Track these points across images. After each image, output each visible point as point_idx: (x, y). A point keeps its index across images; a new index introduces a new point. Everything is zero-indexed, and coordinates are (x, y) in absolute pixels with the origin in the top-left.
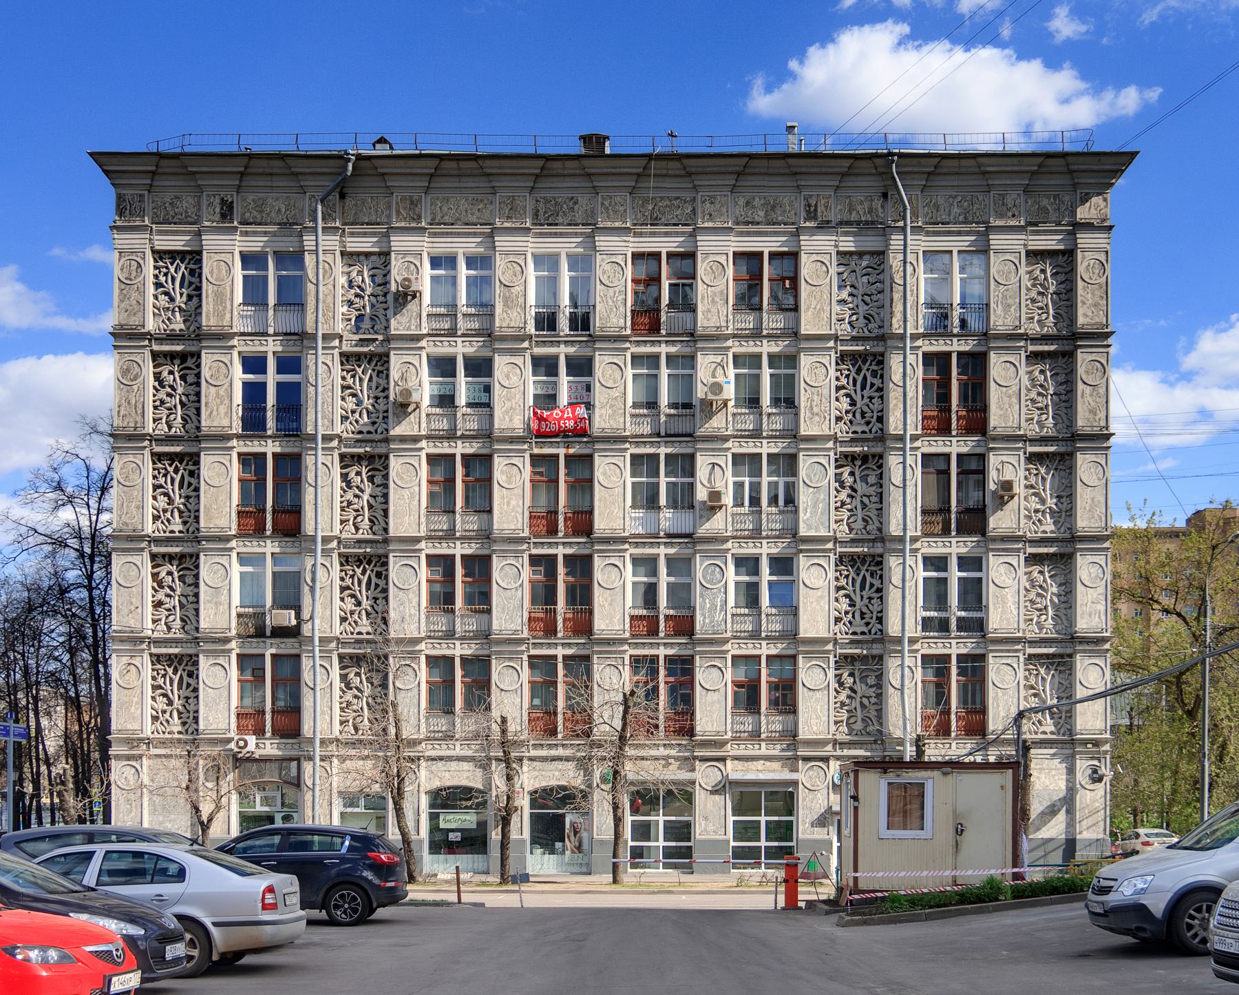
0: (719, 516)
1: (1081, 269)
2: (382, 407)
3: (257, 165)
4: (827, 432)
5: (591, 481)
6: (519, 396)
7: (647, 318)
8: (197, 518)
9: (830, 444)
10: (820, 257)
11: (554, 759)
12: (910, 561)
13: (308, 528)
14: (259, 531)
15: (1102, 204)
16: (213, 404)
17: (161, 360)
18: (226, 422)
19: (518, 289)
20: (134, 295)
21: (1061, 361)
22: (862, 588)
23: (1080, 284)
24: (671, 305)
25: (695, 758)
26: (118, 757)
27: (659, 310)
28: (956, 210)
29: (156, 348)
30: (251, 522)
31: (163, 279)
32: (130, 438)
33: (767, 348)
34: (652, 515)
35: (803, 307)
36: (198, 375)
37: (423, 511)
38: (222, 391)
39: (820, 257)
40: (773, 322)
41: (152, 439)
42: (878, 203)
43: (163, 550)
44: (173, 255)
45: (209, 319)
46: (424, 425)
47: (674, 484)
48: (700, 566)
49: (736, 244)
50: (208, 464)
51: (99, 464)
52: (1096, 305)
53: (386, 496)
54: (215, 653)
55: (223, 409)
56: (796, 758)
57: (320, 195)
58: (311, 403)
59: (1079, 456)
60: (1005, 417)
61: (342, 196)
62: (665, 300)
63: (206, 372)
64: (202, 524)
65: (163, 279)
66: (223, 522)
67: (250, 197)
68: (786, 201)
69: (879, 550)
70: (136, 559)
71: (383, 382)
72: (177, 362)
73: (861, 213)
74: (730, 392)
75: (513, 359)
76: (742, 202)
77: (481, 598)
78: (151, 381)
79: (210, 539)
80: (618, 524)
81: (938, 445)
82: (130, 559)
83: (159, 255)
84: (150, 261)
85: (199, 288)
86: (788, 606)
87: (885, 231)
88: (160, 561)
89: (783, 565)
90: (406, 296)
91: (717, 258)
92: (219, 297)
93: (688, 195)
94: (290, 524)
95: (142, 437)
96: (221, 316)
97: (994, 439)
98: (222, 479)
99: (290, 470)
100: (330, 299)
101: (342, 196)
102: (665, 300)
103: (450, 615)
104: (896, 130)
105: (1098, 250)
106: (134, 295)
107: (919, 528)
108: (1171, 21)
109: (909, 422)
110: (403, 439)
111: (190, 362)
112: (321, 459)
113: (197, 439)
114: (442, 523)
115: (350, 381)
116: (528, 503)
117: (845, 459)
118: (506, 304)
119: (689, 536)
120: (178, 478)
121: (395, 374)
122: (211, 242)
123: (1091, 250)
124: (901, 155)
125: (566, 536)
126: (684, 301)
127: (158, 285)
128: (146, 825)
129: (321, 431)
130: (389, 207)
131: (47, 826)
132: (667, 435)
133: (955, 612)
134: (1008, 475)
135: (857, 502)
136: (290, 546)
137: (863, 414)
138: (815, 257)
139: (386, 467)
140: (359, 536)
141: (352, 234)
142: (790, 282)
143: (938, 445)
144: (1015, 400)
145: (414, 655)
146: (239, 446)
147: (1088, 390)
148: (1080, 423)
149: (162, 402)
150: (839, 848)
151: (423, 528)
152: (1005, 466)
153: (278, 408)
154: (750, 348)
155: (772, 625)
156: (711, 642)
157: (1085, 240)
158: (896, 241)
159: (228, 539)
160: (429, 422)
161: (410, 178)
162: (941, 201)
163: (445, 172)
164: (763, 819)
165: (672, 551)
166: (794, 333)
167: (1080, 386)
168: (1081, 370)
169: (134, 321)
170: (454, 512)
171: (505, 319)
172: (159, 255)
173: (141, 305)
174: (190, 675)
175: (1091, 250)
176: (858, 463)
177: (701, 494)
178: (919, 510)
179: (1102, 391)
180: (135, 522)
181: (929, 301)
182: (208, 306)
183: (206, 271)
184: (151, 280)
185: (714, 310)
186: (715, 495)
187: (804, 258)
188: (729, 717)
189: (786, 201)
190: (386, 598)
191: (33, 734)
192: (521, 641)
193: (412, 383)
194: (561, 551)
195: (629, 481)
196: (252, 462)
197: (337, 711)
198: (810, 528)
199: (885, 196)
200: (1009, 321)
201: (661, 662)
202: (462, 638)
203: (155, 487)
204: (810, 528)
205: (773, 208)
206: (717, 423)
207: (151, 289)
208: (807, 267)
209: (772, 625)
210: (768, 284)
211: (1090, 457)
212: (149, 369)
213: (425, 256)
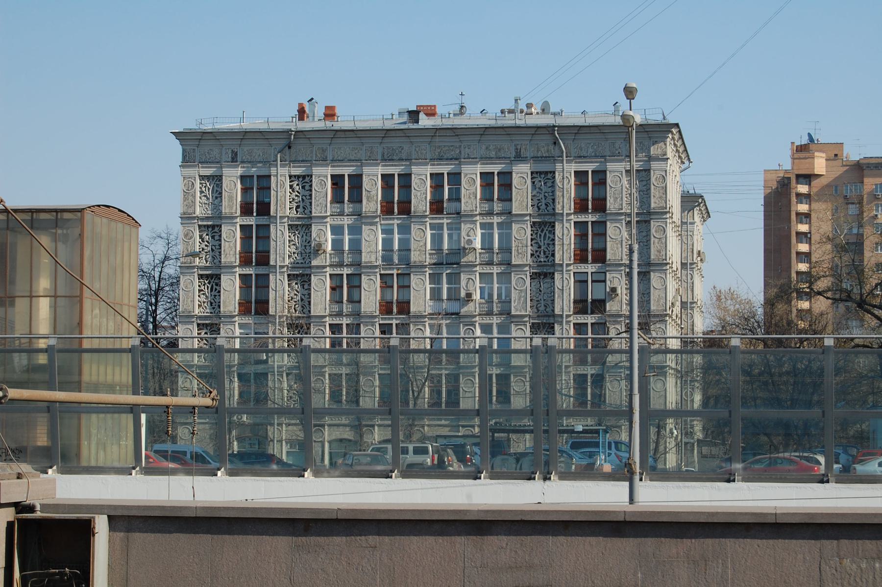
0: (471, 304)
1: (653, 180)
2: (308, 251)
3: (339, 134)
4: (525, 263)
5: (605, 234)
6: (374, 245)
8: (219, 306)
9: (527, 268)
10: (521, 174)
11: (338, 425)
12: (566, 225)
13: (271, 311)
14: (390, 312)
15: (664, 146)
16: (227, 251)
17: (534, 175)
18: (233, 260)
19: (373, 193)
20: (190, 198)
21: (644, 225)
22: (212, 290)
23: (652, 187)
24: (449, 200)
25: (459, 426)
27: (443, 202)
28: (590, 150)
29: (200, 223)
30: (245, 308)
31: (204, 189)
32: (188, 267)
34: (437, 303)
35: (514, 200)
36: (220, 236)
37: (328, 302)
38: (231, 245)
39: (521, 174)
41: (198, 218)
42: (551, 147)
43: (205, 223)
44: (208, 178)
46: (328, 260)
47: (434, 288)
48: (414, 228)
50: (225, 280)
52: (660, 197)
53: (309, 294)
54: (372, 224)
55: (232, 253)
56: (459, 426)
57: (279, 147)
58: (275, 500)
59: (652, 273)
60: (615, 254)
61: (290, 148)
62: (446, 196)
63: (224, 235)
64: (222, 309)
65: (204, 189)
66: (231, 308)
67: (245, 149)
68: (506, 147)
69: (552, 321)
70: (190, 327)
71: (308, 239)
72: (210, 229)
73: (543, 152)
74: (478, 244)
75: (372, 227)
76: (484, 147)
78: (198, 239)
79: (225, 317)
80: (422, 309)
82: (187, 326)
83: (202, 177)
84: (198, 181)
85: (221, 193)
86: (355, 301)
87: (553, 159)
88: (293, 179)
90: (318, 250)
92: (231, 198)
93: (458, 144)
95: (194, 267)
96: (231, 208)
97: (609, 265)
98: (231, 290)
100: (283, 199)
101: (290, 148)
102: (446, 196)
103: (491, 203)
104: (866, 508)
105: (661, 170)
106: (190, 198)
107: (572, 309)
108: (451, 469)
109: (110, 347)
110: (318, 267)
111: (216, 229)
112: (278, 277)
113: (220, 267)
114: (336, 308)
115: (293, 238)
116: (378, 297)
118: (368, 200)
119: (457, 314)
120: (543, 235)
121: (314, 235)
123: (658, 170)
124: (559, 127)
125: (399, 214)
126: (456, 197)
127: (201, 192)
128: (327, 406)
129: (279, 264)
130: (312, 152)
132: (447, 264)
133: (347, 259)
134: (616, 284)
135: (542, 196)
136: (261, 319)
137: (544, 253)
138: (520, 175)
139: (310, 280)
140: (298, 216)
141: (294, 167)
143: (582, 218)
144: (619, 246)
145: (373, 324)
146: (240, 221)
147: (656, 240)
148: (652, 257)
149: (292, 298)
151: (328, 310)
152: (616, 280)
154: (487, 220)
155: (347, 259)
156: (467, 367)
157: (654, 165)
158: (559, 166)
159: (234, 316)
160: (331, 258)
161: (39, 398)
162: (583, 145)
164: (395, 272)
165: (448, 322)
166: (359, 214)
167: (652, 239)
168: (653, 231)
169: (190, 211)
170: (493, 200)
171: (415, 257)
172: (202, 177)
173: (194, 202)
174: (217, 285)
175: (658, 170)
176: (301, 179)
177: (463, 294)
178: (572, 301)
179: (664, 241)
180: (190, 308)
181: (578, 298)
182: (225, 202)
183: (224, 186)
184: (198, 190)
185: (470, 202)
186: (469, 295)
187: (514, 175)
189: (506, 147)
190: (554, 244)
192: (375, 317)
193: (323, 239)
194: (444, 372)
195: (428, 287)
196: (244, 278)
197: (530, 201)
198: (517, 310)
199: (555, 143)
200: (617, 206)
201: (589, 377)
202: (496, 365)
203: (200, 291)
204: (517, 310)
205: (500, 150)
206: (470, 258)
207: (198, 194)
208: (516, 180)
210: (498, 187)
211: (657, 274)
212: (197, 234)
213: (477, 325)
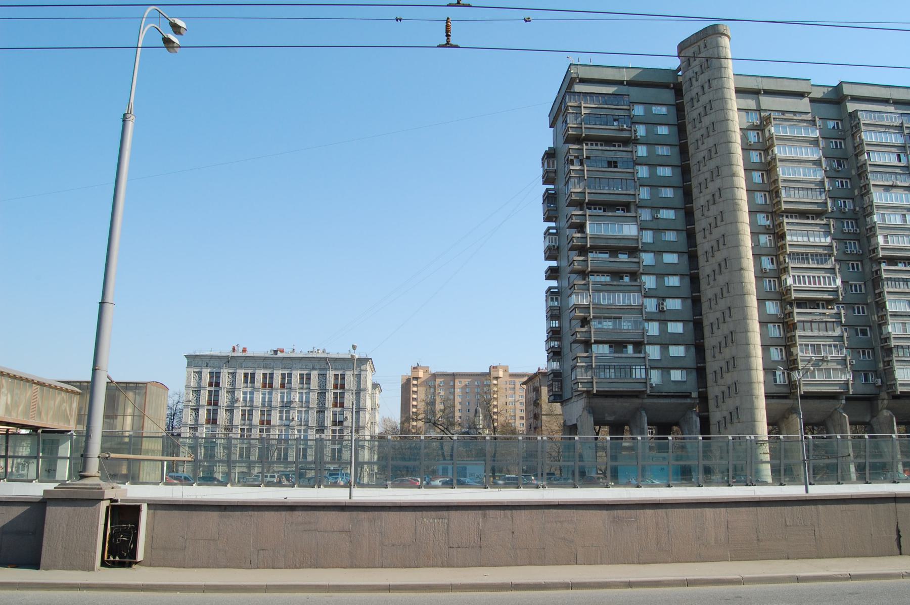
7: (283, 386)
10: (314, 374)
26: (895, 315)
30: (208, 422)
33: (304, 391)
39: (314, 374)
40: (305, 386)
45: (202, 384)
49: (281, 372)
51: (420, 417)
77: (253, 382)
81: (336, 391)
89: (269, 411)
90: (237, 401)
91: (296, 374)
94: (214, 421)
98: (203, 415)
99: (217, 393)
117: (317, 412)
122: (204, 370)
131: (807, 285)
133: (248, 404)
142: (309, 379)
143: (336, 391)
150: (823, 438)
153: (214, 402)
155: (248, 404)
163: (893, 150)
188: (616, 170)
191: (611, 90)
206: (294, 405)
209: (247, 422)
